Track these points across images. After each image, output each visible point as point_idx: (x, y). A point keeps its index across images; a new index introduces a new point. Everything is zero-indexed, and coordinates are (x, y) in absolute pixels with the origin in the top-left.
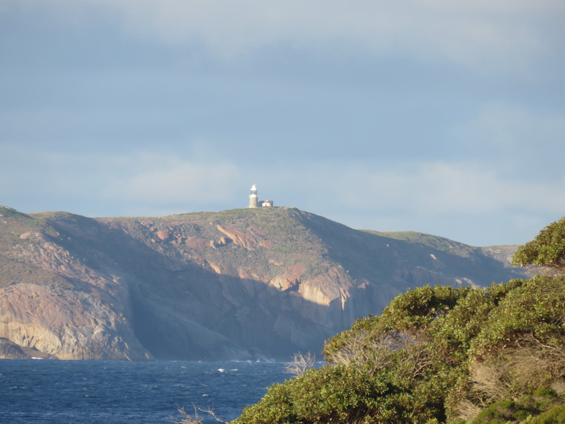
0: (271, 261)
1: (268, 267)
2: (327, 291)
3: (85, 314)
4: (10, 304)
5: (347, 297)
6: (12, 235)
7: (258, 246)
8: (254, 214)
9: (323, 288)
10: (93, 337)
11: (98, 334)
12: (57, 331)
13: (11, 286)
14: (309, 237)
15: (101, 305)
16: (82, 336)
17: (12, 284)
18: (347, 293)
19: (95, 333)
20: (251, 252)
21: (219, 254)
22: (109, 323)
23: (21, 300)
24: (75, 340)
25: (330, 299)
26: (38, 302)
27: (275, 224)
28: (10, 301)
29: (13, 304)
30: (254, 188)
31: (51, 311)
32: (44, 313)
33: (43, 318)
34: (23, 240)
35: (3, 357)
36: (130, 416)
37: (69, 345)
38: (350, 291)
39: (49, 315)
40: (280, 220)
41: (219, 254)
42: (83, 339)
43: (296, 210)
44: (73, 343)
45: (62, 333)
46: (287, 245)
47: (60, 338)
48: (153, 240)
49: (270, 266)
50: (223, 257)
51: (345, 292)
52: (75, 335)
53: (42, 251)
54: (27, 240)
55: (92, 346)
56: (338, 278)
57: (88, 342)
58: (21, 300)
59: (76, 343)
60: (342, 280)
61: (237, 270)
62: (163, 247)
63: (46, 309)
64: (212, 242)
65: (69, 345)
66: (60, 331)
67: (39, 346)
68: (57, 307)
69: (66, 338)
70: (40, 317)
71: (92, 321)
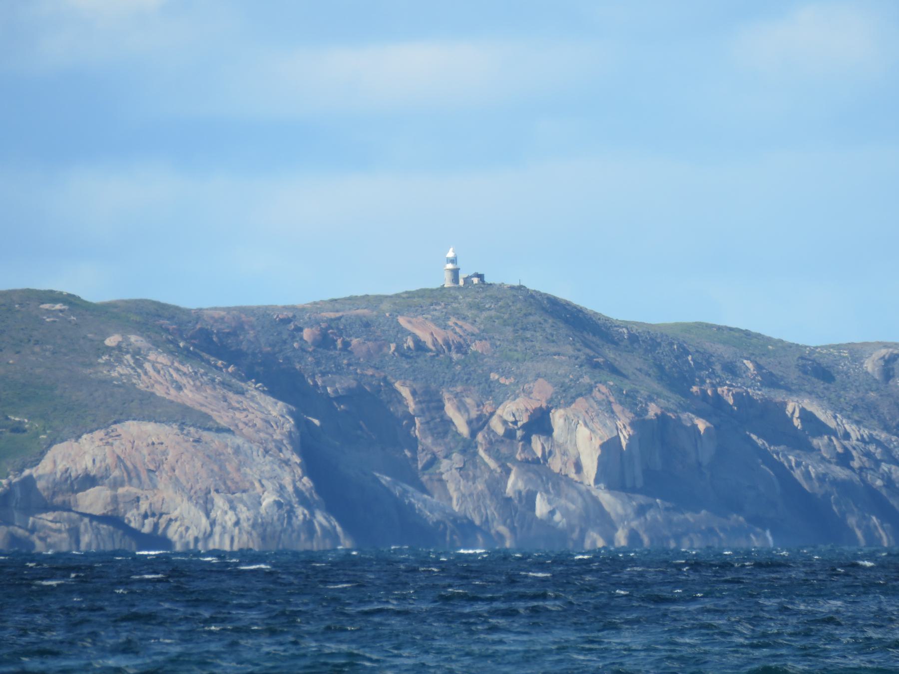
0: (494, 376)
1: (489, 387)
2: (597, 426)
3: (242, 470)
4: (118, 457)
5: (629, 435)
6: (92, 340)
7: (469, 352)
8: (456, 298)
9: (587, 421)
10: (262, 510)
11: (269, 506)
12: (201, 501)
13: (114, 426)
14: (552, 335)
15: (264, 457)
16: (244, 509)
17: (115, 423)
18: (628, 428)
19: (264, 504)
20: (457, 363)
21: (407, 366)
22: (282, 488)
23: (137, 449)
24: (234, 519)
25: (601, 438)
26: (164, 453)
27: (493, 313)
28: (118, 451)
29: (122, 457)
30: (450, 254)
31: (187, 467)
32: (177, 472)
33: (177, 480)
34: (112, 348)
35: (2, 558)
36: (766, 651)
37: (224, 528)
38: (632, 424)
39: (185, 474)
40: (501, 307)
41: (407, 366)
42: (245, 513)
43: (521, 288)
44: (230, 524)
45: (209, 506)
46: (518, 348)
47: (208, 515)
48: (295, 345)
49: (492, 385)
50: (414, 371)
51: (625, 427)
52: (233, 508)
53: (148, 366)
54: (119, 347)
55: (260, 526)
56: (610, 403)
57: (255, 519)
58: (137, 449)
59: (237, 523)
60: (617, 408)
61: (438, 392)
62: (313, 357)
63: (179, 463)
64: (393, 347)
65: (224, 528)
66: (206, 502)
67: (173, 533)
68: (196, 460)
69: (216, 514)
70: (171, 478)
71: (257, 485)
